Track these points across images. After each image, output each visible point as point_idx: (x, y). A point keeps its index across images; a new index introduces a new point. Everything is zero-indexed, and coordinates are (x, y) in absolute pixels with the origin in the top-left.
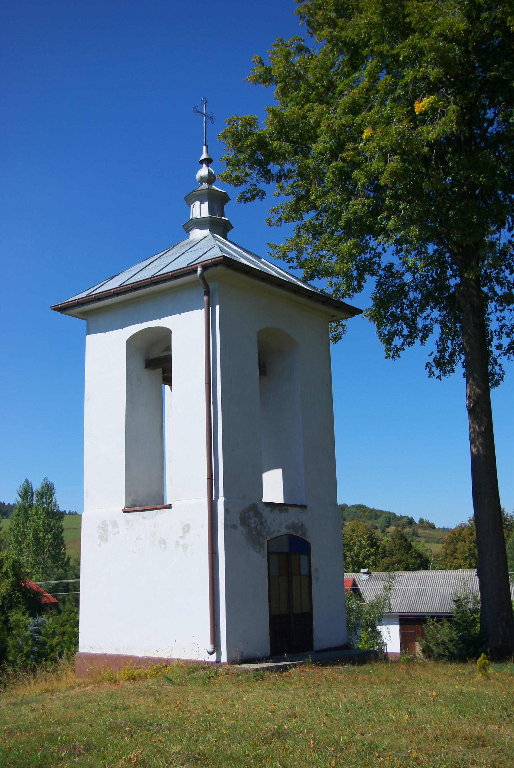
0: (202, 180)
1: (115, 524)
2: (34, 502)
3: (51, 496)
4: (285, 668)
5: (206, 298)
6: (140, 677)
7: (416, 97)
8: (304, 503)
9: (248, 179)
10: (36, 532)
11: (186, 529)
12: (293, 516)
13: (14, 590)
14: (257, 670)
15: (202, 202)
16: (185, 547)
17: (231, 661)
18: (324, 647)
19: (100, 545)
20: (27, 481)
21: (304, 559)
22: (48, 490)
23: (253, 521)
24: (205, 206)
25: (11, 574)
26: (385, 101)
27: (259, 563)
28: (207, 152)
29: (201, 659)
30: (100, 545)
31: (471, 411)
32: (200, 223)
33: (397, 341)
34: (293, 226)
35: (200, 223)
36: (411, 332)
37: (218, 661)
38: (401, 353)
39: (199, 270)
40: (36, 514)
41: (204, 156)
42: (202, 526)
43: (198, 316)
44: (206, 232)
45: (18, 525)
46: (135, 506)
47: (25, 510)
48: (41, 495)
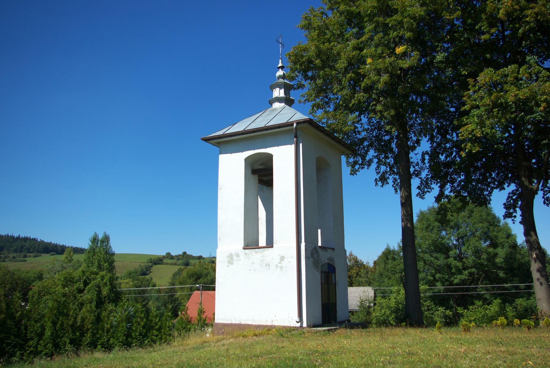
0: (280, 77)
1: (238, 255)
2: (99, 245)
3: (108, 241)
4: (335, 329)
5: (295, 139)
6: (260, 335)
7: (397, 45)
9: (296, 78)
10: (99, 261)
11: (282, 258)
12: (329, 254)
13: (110, 293)
14: (325, 330)
15: (280, 89)
16: (281, 268)
17: (309, 326)
18: (341, 320)
19: (228, 266)
20: (96, 234)
21: (333, 275)
22: (106, 239)
23: (315, 255)
24: (282, 91)
25: (108, 284)
27: (318, 276)
28: (282, 63)
29: (292, 325)
30: (228, 266)
31: (402, 204)
32: (279, 100)
33: (357, 167)
34: (311, 104)
35: (279, 100)
36: (362, 162)
37: (301, 326)
38: (357, 173)
39: (295, 125)
40: (100, 252)
41: (280, 65)
43: (291, 148)
44: (283, 105)
45: (89, 258)
46: (247, 246)
47: (92, 250)
48: (102, 242)
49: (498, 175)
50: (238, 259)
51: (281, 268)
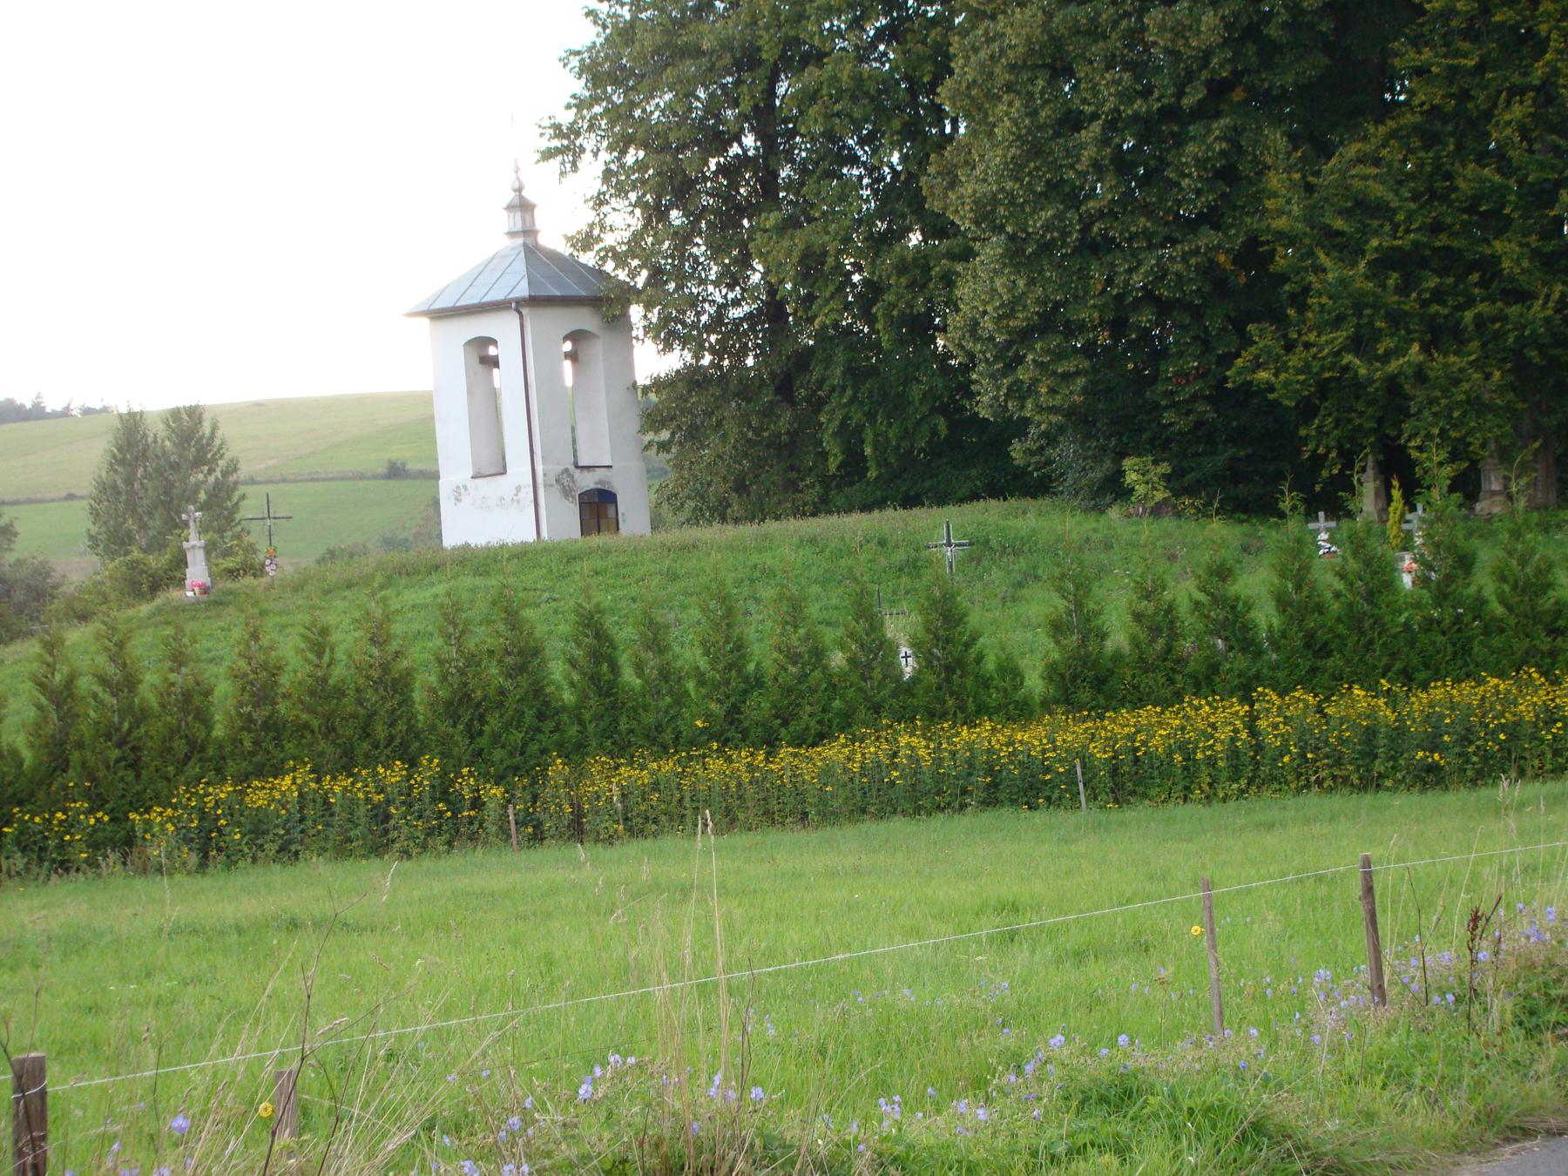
1: (465, 488)
11: (518, 489)
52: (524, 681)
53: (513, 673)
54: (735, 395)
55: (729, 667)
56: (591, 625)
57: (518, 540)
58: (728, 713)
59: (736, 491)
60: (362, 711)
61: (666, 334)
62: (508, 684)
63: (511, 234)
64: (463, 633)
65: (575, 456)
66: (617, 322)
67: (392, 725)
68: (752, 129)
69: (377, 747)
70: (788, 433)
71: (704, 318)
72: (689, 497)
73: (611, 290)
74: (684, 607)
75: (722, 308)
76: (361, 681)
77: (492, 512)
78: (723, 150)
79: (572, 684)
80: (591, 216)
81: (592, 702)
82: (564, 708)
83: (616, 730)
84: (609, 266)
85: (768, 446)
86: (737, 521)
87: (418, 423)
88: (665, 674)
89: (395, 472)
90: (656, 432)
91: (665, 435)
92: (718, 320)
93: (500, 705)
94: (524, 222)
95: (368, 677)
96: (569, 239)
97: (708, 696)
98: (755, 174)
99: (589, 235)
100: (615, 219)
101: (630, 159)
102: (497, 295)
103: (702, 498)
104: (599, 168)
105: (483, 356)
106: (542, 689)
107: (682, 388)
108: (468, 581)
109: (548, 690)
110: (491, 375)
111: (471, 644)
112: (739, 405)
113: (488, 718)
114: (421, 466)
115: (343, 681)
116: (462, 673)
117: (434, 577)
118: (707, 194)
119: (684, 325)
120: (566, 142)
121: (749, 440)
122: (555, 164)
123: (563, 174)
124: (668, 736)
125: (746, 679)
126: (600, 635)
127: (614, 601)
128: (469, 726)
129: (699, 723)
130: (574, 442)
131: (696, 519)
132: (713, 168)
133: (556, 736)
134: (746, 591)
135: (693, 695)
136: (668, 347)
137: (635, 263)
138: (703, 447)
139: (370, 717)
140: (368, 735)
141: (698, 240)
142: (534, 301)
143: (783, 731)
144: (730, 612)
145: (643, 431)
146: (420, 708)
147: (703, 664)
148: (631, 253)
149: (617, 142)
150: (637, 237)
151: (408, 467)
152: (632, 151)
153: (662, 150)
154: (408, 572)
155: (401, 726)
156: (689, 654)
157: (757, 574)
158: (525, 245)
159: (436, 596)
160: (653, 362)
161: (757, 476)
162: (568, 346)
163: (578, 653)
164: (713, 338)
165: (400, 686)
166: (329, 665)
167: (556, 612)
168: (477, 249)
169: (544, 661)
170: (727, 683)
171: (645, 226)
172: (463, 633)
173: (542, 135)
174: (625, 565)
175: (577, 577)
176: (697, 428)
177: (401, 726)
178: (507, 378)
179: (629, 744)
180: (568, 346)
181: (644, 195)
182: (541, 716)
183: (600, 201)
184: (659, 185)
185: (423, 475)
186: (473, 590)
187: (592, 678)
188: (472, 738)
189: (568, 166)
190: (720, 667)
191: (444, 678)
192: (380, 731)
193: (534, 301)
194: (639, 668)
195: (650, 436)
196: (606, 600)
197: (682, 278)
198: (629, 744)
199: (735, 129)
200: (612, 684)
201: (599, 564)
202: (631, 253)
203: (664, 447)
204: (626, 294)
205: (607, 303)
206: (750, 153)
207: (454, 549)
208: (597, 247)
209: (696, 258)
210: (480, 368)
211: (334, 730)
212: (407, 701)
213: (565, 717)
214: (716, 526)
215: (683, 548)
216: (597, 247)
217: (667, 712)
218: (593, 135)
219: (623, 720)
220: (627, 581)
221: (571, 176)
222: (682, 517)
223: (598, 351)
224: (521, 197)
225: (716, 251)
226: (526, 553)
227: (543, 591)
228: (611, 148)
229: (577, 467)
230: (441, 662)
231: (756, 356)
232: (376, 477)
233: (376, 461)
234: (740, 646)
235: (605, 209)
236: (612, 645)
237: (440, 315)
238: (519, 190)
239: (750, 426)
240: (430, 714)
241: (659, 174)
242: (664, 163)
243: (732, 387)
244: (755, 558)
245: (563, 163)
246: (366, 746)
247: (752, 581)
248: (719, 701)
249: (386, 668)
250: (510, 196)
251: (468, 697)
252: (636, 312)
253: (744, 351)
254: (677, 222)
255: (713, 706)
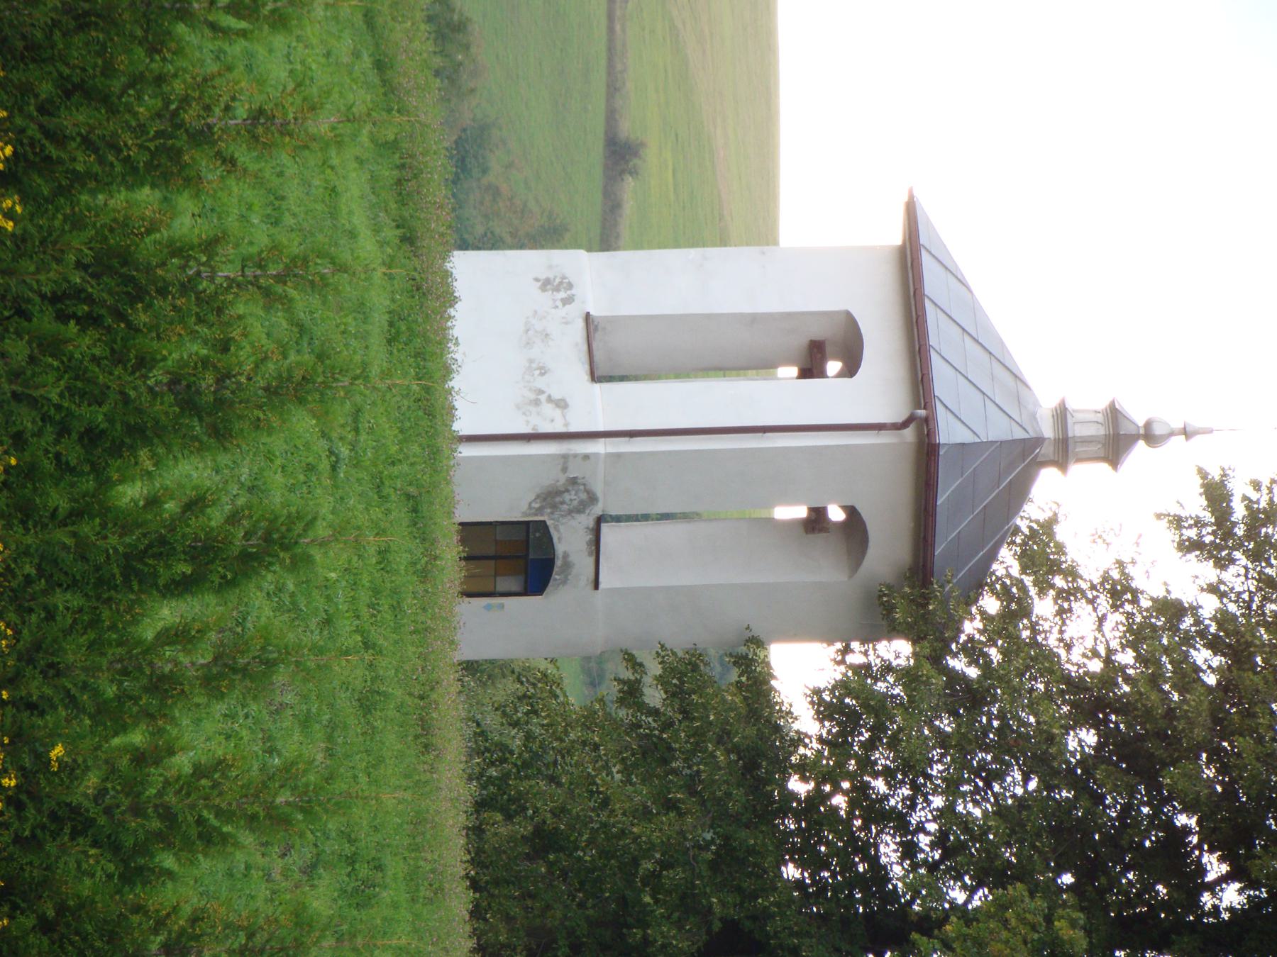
1: (568, 301)
8: (601, 586)
11: (562, 404)
18: (487, 562)
19: (537, 280)
21: (512, 583)
26: (868, 797)
30: (537, 280)
42: (566, 425)
49: (992, 740)
50: (559, 304)
51: (537, 403)
52: (164, 407)
53: (183, 390)
54: (727, 838)
55: (168, 815)
56: (271, 544)
57: (459, 403)
58: (75, 810)
59: (538, 831)
60: (116, 85)
61: (848, 707)
62: (157, 376)
63: (1061, 414)
64: (267, 292)
65: (618, 519)
66: (880, 616)
67: (87, 143)
68: (1255, 904)
69: (42, 110)
70: (646, 941)
71: (880, 785)
72: (529, 737)
73: (944, 602)
74: (305, 722)
75: (900, 822)
76: (178, 86)
77: (518, 348)
78: (1212, 839)
79: (153, 502)
80: (1091, 572)
81: (113, 540)
82: (105, 483)
83: (53, 585)
84: (991, 604)
85: (623, 902)
86: (476, 831)
87: (724, 210)
88: (165, 687)
89: (621, 155)
90: (660, 679)
91: (654, 696)
92: (876, 813)
93: (118, 358)
94: (1086, 441)
95: (185, 101)
96: (1048, 526)
97: (112, 771)
98: (1164, 905)
99: (1055, 567)
100: (1082, 623)
101: (1201, 655)
102: (943, 380)
103: (526, 765)
104: (1186, 593)
105: (825, 348)
106: (147, 442)
107: (744, 734)
108: (379, 301)
109: (143, 454)
110: (788, 362)
111: (245, 307)
112: (705, 847)
113: (93, 334)
114: (629, 207)
115: (179, 52)
116: (187, 287)
117: (391, 234)
118: (1127, 809)
119: (870, 745)
120: (1240, 531)
121: (635, 862)
122: (1196, 506)
123: (1178, 522)
124: (35, 687)
125: (142, 849)
126: (248, 564)
127: (327, 585)
128: (78, 294)
129: (58, 751)
130: (646, 517)
131: (484, 748)
132: (1182, 820)
133: (48, 465)
134: (332, 847)
135: (116, 741)
136: (824, 711)
137: (995, 654)
138: (626, 771)
139: (105, 99)
140: (68, 94)
141: (1033, 785)
142: (927, 454)
143: (29, 921)
144: (279, 820)
145: (663, 652)
146: (120, 199)
147: (182, 763)
148: (1014, 648)
149: (1237, 633)
150: (1045, 661)
151: (629, 180)
152: (1217, 661)
153: (1216, 721)
154: (405, 182)
155: (83, 161)
156: (200, 735)
157: (364, 871)
158: (1039, 441)
159: (352, 235)
160: (801, 673)
161: (564, 874)
162: (836, 514)
163: (216, 517)
164: (839, 801)
165: (166, 163)
166: (213, 27)
167: (310, 468)
168: (1046, 337)
169: (202, 449)
170: (137, 811)
171: (1067, 679)
172: (267, 292)
173: (1257, 485)
174: (396, 608)
175: (376, 513)
176: (665, 761)
177: (83, 161)
178: (782, 396)
179: (24, 611)
180: (836, 514)
181: (1128, 679)
182: (91, 437)
183: (1119, 591)
184: (1148, 712)
185: (612, 207)
186: (362, 310)
187: (163, 541)
188: (54, 299)
189: (1192, 533)
190: (171, 798)
191: (178, 250)
192: (76, 118)
193: (927, 454)
194: (180, 636)
195: (655, 669)
196: (329, 564)
197: (959, 746)
198: (24, 611)
199: (1255, 868)
200: (148, 582)
201: (401, 560)
202: (1014, 648)
203: (631, 693)
204: (933, 635)
205: (917, 597)
206: (1207, 898)
207: (448, 274)
208: (1028, 580)
209: (1000, 776)
210: (799, 342)
211: (81, 27)
212: (134, 175)
213: (89, 484)
214: (466, 792)
215: (425, 726)
216: (1028, 580)
217: (85, 687)
218: (1252, 585)
219: (76, 601)
220: (365, 612)
221: (1169, 537)
222: (492, 721)
223: (823, 572)
224: (1132, 439)
225: (1012, 817)
226: (430, 414)
227: (353, 446)
228: (1223, 618)
229: (599, 520)
230: (210, 246)
231: (799, 884)
232: (611, 117)
233: (643, 119)
234: (210, 839)
235: (1104, 603)
236: (227, 584)
237: (910, 261)
238: (1150, 436)
239: (665, 865)
240: (105, 219)
241: (1170, 713)
242: (1191, 723)
243: (743, 834)
244: (395, 867)
245: (1199, 523)
246: (46, 89)
247: (351, 860)
248: (101, 793)
249: (203, 137)
250: (1138, 415)
251: (137, 295)
252: (899, 651)
253: (811, 861)
254: (1072, 744)
255: (92, 780)
